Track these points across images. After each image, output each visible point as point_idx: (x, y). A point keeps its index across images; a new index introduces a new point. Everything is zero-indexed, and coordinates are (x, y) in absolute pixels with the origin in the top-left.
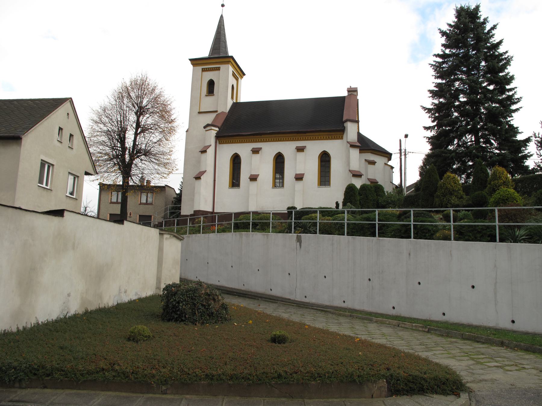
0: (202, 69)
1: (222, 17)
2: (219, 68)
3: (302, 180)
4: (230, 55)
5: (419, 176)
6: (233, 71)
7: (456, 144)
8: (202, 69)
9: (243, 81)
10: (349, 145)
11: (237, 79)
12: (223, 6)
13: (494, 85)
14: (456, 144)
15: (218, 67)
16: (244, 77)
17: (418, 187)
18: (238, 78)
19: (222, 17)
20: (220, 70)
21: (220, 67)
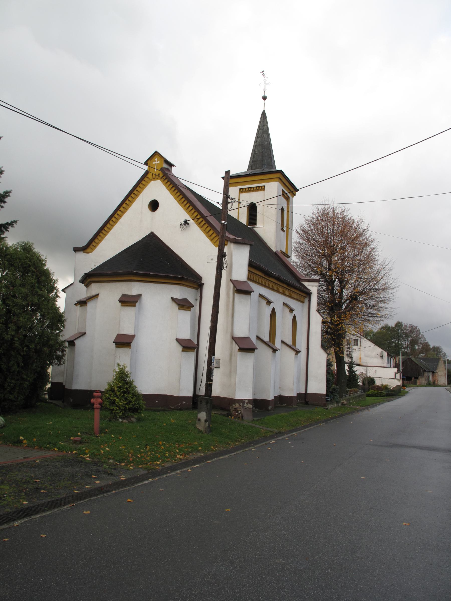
0: (240, 189)
1: (264, 115)
2: (263, 188)
3: (254, 352)
4: (278, 168)
5: (75, 343)
6: (282, 189)
7: (347, 300)
8: (240, 189)
9: (297, 199)
10: (238, 348)
11: (287, 199)
12: (264, 98)
13: (43, 396)
14: (347, 300)
15: (262, 186)
16: (297, 193)
17: (43, 338)
18: (289, 197)
19: (264, 115)
20: (264, 189)
21: (264, 186)
